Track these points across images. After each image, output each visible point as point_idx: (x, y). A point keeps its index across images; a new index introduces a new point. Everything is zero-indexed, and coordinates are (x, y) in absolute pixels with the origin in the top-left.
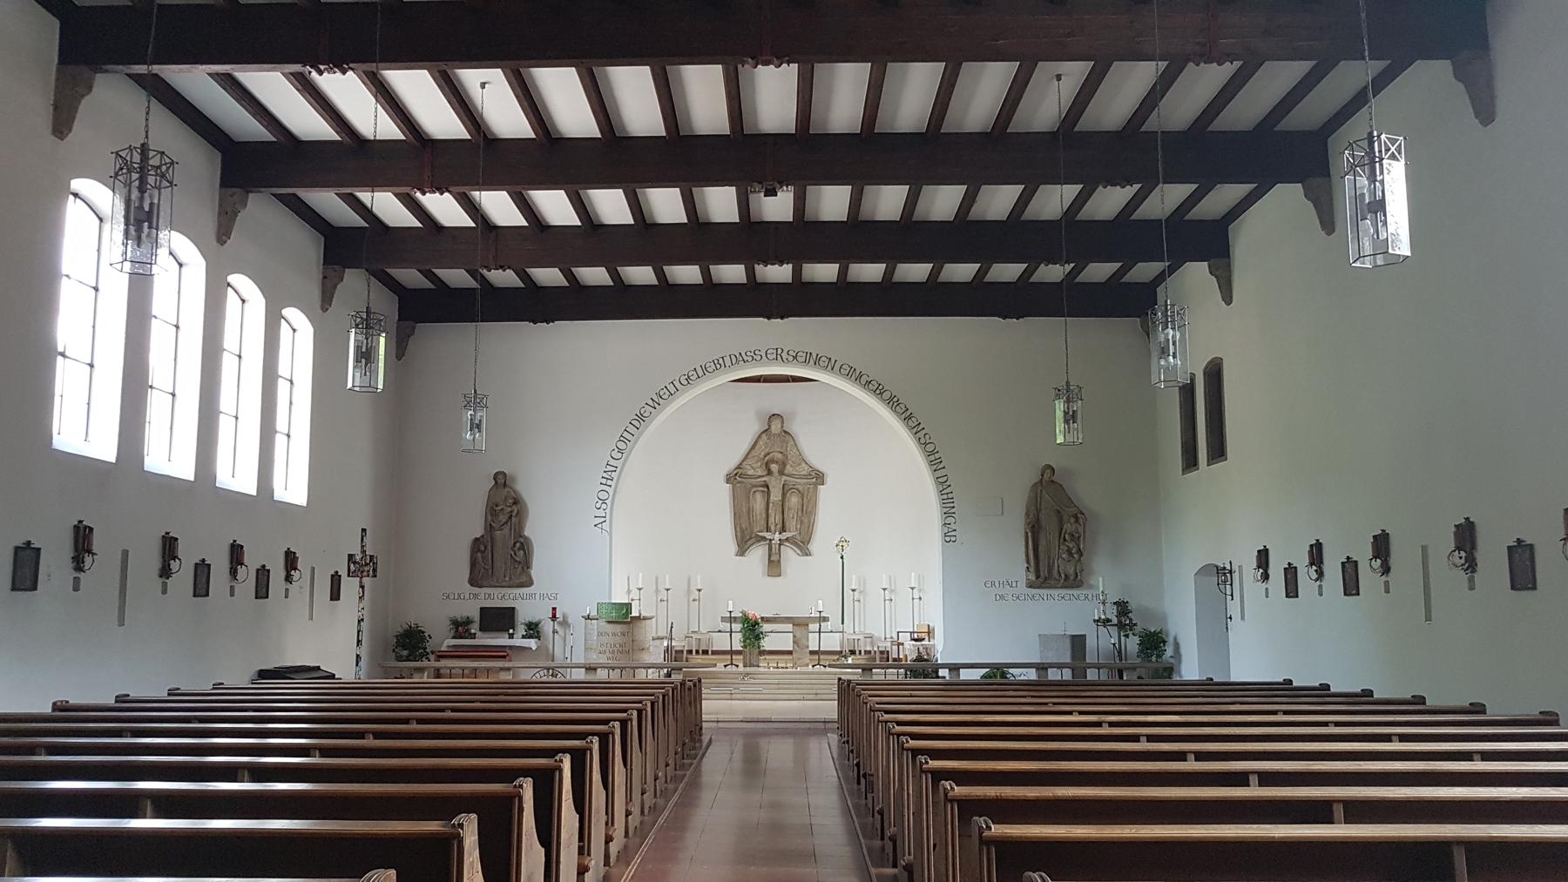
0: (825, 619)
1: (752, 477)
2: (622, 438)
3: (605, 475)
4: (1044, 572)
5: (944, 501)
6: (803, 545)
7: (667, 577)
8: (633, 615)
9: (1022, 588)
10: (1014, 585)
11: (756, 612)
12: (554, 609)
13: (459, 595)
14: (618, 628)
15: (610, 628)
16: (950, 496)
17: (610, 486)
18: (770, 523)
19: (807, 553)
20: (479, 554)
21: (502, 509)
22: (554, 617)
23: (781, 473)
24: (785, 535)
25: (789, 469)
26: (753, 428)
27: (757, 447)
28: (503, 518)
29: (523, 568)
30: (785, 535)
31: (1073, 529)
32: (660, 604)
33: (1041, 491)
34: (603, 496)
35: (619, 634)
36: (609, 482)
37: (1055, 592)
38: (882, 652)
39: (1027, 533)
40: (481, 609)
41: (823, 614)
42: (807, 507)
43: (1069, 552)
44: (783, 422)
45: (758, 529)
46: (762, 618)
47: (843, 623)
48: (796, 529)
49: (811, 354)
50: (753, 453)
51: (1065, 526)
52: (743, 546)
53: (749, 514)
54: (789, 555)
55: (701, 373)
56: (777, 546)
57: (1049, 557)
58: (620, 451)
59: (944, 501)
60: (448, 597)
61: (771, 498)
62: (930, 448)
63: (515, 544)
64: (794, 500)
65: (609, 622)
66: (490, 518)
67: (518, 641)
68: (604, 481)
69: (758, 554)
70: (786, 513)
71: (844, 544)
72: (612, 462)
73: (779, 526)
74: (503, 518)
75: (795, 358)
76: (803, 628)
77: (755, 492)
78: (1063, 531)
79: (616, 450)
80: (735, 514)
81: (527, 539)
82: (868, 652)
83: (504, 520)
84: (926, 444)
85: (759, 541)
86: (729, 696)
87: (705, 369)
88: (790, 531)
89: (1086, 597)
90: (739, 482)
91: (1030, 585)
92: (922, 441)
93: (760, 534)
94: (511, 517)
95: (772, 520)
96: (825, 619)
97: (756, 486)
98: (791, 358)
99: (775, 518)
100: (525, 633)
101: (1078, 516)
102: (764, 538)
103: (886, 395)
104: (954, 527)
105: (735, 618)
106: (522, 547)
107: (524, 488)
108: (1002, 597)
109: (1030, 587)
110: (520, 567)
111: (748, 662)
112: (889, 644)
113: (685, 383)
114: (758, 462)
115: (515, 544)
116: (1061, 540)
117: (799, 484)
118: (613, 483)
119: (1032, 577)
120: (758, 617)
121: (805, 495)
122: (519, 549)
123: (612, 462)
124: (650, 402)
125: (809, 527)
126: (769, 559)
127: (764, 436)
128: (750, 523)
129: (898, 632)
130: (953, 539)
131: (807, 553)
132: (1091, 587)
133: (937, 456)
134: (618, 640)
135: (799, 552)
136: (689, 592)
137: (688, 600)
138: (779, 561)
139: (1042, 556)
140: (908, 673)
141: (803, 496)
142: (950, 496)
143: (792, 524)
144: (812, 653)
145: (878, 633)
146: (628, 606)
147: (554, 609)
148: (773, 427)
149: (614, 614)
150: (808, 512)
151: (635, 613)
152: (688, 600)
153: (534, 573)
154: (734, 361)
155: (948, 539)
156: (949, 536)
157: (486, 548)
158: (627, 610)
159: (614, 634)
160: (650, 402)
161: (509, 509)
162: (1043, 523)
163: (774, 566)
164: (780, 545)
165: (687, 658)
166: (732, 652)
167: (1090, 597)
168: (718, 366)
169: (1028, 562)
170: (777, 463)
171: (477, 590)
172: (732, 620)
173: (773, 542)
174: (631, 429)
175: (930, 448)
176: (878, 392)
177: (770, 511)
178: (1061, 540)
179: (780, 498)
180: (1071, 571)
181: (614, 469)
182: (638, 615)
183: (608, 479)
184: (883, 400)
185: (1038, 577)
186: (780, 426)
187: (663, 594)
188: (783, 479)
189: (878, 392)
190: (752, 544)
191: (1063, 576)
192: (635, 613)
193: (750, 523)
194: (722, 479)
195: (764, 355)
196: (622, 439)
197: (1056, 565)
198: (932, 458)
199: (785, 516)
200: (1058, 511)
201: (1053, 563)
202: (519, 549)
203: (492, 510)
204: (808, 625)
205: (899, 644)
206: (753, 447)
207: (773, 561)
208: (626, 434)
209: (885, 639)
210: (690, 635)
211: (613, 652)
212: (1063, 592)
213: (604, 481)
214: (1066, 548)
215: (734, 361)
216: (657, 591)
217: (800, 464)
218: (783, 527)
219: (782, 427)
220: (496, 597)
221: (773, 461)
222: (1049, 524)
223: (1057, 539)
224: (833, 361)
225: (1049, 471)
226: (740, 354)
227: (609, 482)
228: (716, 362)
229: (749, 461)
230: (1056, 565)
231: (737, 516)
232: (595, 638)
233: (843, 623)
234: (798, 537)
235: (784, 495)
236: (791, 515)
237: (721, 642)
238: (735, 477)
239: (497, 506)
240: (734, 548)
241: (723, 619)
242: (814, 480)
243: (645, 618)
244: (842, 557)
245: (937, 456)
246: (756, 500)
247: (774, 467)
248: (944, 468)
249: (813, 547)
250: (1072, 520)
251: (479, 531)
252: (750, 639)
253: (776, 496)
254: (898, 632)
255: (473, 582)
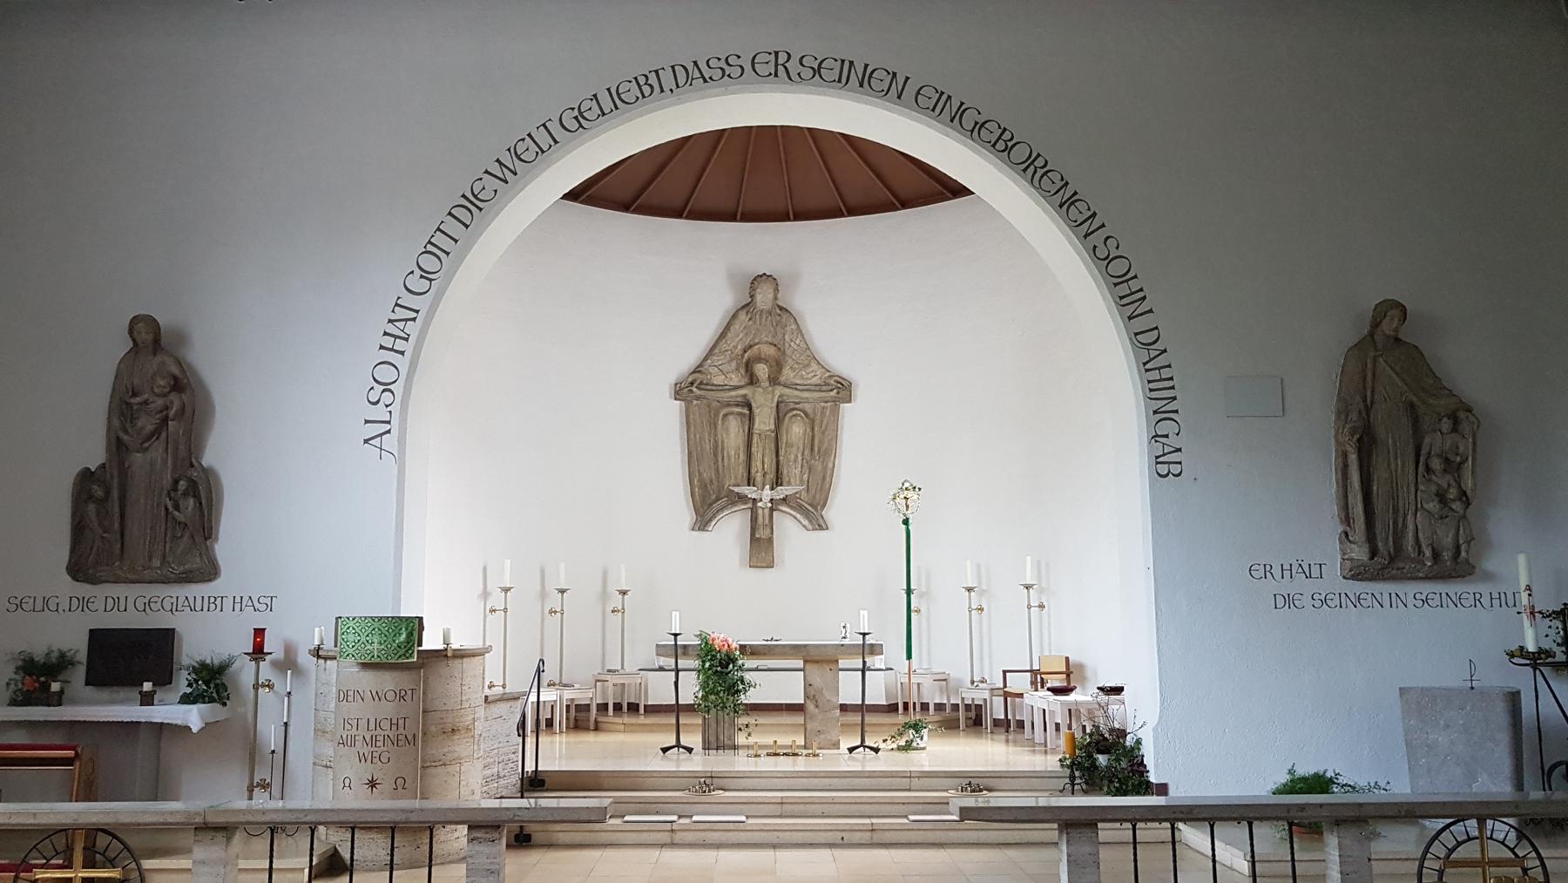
0: (875, 650)
1: (722, 388)
2: (430, 248)
3: (391, 329)
4: (1387, 543)
5: (1152, 386)
6: (813, 510)
7: (562, 565)
8: (426, 646)
9: (1334, 579)
10: (1315, 572)
11: (729, 634)
12: (259, 632)
13: (46, 601)
14: (388, 681)
15: (368, 681)
16: (1165, 373)
17: (402, 353)
18: (753, 471)
19: (820, 525)
20: (92, 507)
21: (146, 403)
22: (258, 652)
23: (774, 381)
24: (782, 491)
25: (787, 374)
26: (723, 301)
27: (729, 335)
28: (147, 423)
29: (192, 537)
30: (782, 491)
31: (1447, 447)
32: (490, 617)
33: (1375, 359)
34: (386, 374)
35: (390, 696)
36: (400, 345)
37: (1408, 589)
38: (968, 707)
39: (1345, 455)
40: (91, 630)
41: (870, 640)
42: (821, 442)
43: (1441, 497)
44: (776, 290)
45: (733, 481)
46: (743, 648)
47: (909, 657)
48: (802, 483)
49: (851, 63)
50: (723, 345)
51: (1427, 440)
52: (705, 513)
53: (715, 455)
54: (788, 528)
55: (607, 104)
56: (767, 511)
57: (1396, 511)
58: (426, 275)
59: (1152, 386)
60: (19, 606)
61: (756, 426)
62: (1118, 267)
63: (176, 482)
64: (796, 430)
65: (365, 666)
66: (116, 423)
67: (168, 711)
68: (388, 342)
69: (731, 527)
70: (782, 452)
71: (910, 494)
72: (408, 300)
73: (771, 476)
74: (147, 423)
75: (817, 71)
76: (827, 668)
77: (725, 416)
78: (1424, 451)
79: (418, 272)
80: (690, 453)
81: (209, 475)
82: (940, 707)
83: (150, 428)
84: (1108, 259)
85: (734, 503)
86: (665, 838)
87: (617, 97)
88: (789, 484)
89: (1477, 601)
90: (698, 398)
91: (1357, 573)
92: (1102, 253)
93: (736, 489)
94: (165, 420)
95: (757, 464)
96: (875, 650)
97: (729, 405)
98: (807, 73)
99: (763, 460)
100: (189, 690)
101: (1459, 415)
102: (742, 498)
103: (1020, 153)
104: (1173, 441)
105: (685, 647)
106: (193, 489)
107: (204, 358)
108: (1289, 601)
109: (1355, 577)
110: (187, 534)
111: (713, 739)
112: (986, 695)
113: (573, 125)
114: (730, 362)
115: (176, 482)
116: (1421, 468)
117: (807, 401)
118: (408, 347)
119: (1360, 553)
120: (734, 645)
121: (817, 423)
122: (185, 494)
123: (408, 300)
124: (496, 170)
125: (824, 478)
126: (753, 534)
127: (743, 316)
128: (717, 470)
129: (1005, 672)
130: (1175, 469)
131: (820, 525)
132: (1488, 577)
133: (1134, 285)
134: (388, 709)
135: (806, 522)
136: (604, 595)
137: (604, 612)
138: (770, 540)
139: (1379, 504)
140: (1077, 774)
141: (813, 422)
142: (1165, 373)
143: (793, 471)
144: (844, 708)
145: (959, 671)
146: (415, 626)
147: (259, 632)
148: (759, 298)
149: (376, 645)
150: (821, 449)
151: (431, 641)
152: (604, 612)
153: (223, 549)
154: (682, 79)
155: (1163, 469)
156: (1165, 464)
157: (108, 492)
158: (410, 634)
159: (377, 696)
160: (496, 170)
161: (160, 402)
162: (1381, 432)
163: (761, 549)
164: (772, 510)
165: (596, 722)
166: (677, 709)
167: (1486, 600)
168: (646, 90)
169: (1347, 519)
170: (766, 361)
171: (85, 590)
172: (678, 651)
173: (760, 504)
174: (452, 227)
175: (1118, 267)
176: (1001, 146)
177: (754, 449)
178: (1421, 468)
179: (773, 427)
180: (1448, 541)
181: (413, 315)
182: (441, 646)
183: (396, 337)
184: (1013, 164)
185: (1374, 553)
186: (771, 296)
187: (554, 601)
188: (777, 393)
189: (1001, 146)
190: (722, 509)
191: (1428, 553)
192: (431, 641)
193: (717, 470)
194: (666, 390)
195: (748, 67)
196: (431, 249)
197: (1411, 527)
198: (1124, 289)
199: (775, 459)
200: (1412, 405)
201: (1405, 525)
202: (185, 494)
203: (124, 407)
204: (837, 661)
205: (1006, 695)
206: (723, 335)
207: (759, 539)
208: (440, 239)
209: (973, 682)
210: (603, 677)
211: (374, 739)
212: (1426, 588)
213: (388, 342)
214: (1433, 488)
215: (682, 79)
216: (543, 595)
217: (808, 365)
218: (777, 479)
219: (776, 298)
220: (130, 606)
221: (759, 359)
222: (1393, 435)
223: (1412, 467)
224: (901, 80)
225: (1396, 312)
226: (695, 63)
227: (400, 345)
228: (642, 80)
229: (718, 359)
230: (1411, 527)
231: (694, 457)
232: (332, 705)
233: (909, 657)
234: (804, 495)
235: (779, 421)
236: (793, 457)
237: (660, 690)
238: (690, 389)
239: (135, 394)
240: (687, 515)
241: (661, 650)
242: (833, 393)
243: (461, 655)
244: (906, 522)
245: (1134, 285)
246: (727, 430)
247: (762, 370)
248: (1150, 311)
249: (832, 513)
250: (1446, 425)
251: (94, 454)
252: (717, 694)
253: (764, 422)
254: (1005, 672)
255: (78, 570)
